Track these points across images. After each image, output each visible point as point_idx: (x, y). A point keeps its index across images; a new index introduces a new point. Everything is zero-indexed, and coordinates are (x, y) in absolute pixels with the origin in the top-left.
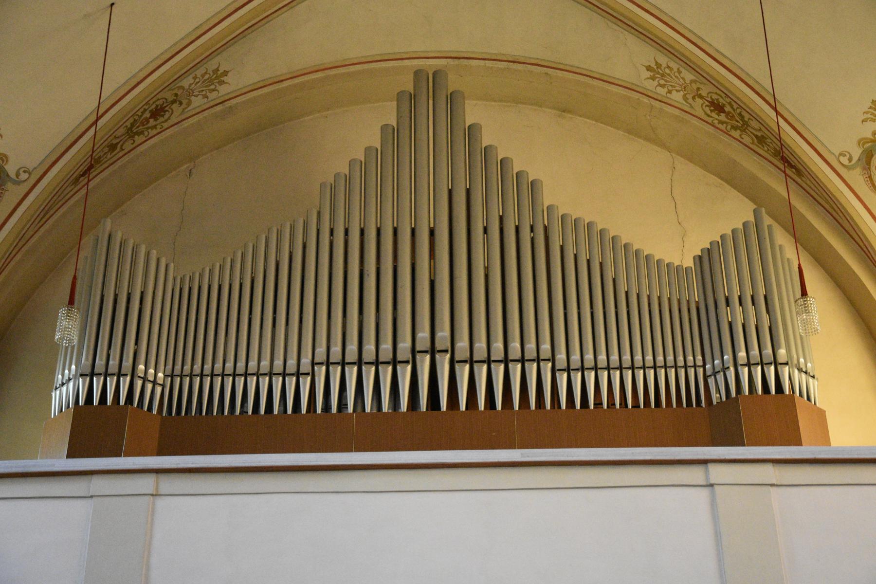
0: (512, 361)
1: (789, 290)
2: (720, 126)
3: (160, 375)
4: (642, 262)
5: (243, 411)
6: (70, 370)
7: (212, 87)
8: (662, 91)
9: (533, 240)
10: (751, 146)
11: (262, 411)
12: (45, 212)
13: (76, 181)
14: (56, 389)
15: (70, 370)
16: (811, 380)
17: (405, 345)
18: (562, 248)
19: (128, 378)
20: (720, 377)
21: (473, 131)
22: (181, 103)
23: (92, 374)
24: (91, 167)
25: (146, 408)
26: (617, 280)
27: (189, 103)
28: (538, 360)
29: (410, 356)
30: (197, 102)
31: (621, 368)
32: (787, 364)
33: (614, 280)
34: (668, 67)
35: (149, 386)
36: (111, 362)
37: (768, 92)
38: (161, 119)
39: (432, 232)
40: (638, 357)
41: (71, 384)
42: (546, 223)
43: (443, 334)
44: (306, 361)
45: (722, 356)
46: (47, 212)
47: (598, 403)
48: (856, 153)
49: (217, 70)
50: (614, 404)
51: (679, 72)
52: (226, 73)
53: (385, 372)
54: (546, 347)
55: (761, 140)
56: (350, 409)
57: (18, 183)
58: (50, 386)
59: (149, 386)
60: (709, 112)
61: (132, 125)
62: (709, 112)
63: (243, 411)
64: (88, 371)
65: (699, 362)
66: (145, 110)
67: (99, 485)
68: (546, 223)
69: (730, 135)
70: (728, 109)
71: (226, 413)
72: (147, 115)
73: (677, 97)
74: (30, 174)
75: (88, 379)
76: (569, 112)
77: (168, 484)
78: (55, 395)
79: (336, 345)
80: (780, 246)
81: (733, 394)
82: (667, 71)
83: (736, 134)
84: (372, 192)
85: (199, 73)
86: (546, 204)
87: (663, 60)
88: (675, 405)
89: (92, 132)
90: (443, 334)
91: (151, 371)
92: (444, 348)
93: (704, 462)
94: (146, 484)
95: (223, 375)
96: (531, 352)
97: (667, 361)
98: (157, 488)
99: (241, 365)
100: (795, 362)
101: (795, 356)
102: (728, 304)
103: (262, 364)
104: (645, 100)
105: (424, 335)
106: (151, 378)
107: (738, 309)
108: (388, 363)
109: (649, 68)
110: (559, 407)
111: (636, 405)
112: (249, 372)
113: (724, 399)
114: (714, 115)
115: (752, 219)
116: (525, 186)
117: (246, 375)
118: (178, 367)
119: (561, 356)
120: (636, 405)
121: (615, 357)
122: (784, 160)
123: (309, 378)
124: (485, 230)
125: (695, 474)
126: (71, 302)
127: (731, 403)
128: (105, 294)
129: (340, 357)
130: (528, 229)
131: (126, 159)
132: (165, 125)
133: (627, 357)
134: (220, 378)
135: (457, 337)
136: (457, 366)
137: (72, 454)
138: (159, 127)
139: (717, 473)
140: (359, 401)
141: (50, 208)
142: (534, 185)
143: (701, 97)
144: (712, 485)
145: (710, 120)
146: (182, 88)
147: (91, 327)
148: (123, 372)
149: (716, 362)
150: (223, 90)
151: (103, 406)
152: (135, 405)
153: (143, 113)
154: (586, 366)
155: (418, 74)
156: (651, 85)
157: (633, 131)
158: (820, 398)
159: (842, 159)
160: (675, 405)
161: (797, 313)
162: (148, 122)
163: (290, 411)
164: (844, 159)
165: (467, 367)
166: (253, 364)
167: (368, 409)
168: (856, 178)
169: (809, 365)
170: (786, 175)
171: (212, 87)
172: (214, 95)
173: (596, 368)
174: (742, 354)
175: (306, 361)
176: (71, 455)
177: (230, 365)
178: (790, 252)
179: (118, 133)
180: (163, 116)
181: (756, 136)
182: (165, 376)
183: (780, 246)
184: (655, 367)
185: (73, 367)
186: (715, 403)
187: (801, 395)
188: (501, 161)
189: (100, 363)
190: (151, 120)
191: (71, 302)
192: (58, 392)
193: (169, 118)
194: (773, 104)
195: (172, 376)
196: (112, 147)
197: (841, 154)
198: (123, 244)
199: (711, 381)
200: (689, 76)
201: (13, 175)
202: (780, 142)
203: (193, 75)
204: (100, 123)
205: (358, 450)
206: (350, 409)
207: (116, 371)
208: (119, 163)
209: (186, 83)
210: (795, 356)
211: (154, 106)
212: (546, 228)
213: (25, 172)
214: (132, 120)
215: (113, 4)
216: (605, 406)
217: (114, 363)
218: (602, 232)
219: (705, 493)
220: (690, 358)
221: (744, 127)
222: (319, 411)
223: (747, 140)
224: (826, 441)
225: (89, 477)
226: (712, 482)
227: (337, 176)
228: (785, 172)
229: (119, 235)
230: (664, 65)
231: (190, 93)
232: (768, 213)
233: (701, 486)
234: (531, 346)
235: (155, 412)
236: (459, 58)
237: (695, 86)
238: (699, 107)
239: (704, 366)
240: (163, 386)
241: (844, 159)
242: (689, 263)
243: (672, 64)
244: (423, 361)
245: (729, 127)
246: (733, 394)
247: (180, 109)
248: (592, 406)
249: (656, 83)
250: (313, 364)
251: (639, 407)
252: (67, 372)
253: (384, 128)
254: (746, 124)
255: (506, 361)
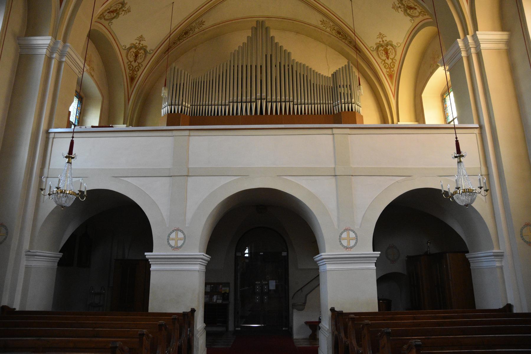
0: (268, 102)
1: (355, 84)
2: (340, 38)
3: (189, 105)
4: (318, 76)
5: (211, 115)
6: (166, 104)
7: (201, 26)
8: (324, 28)
9: (288, 69)
10: (348, 44)
11: (216, 115)
12: (157, 62)
13: (165, 53)
14: (163, 109)
15: (166, 104)
16: (360, 108)
17: (254, 97)
18: (296, 71)
19: (181, 106)
20: (337, 107)
21: (272, 38)
22: (192, 31)
23: (171, 105)
24: (169, 49)
25: (186, 114)
26: (311, 80)
27: (195, 30)
28: (289, 102)
29: (255, 100)
30: (197, 30)
31: (320, 104)
32: (354, 103)
33: (310, 80)
34: (326, 21)
35: (186, 108)
36: (176, 102)
37: (352, 29)
38: (187, 35)
39: (261, 67)
40: (316, 101)
41: (166, 108)
42: (292, 64)
43: (264, 94)
44: (227, 101)
45: (338, 101)
46: (158, 62)
47: (305, 113)
48: (375, 47)
49: (202, 21)
50: (309, 114)
51: (329, 23)
52: (204, 22)
53: (239, 104)
54: (291, 98)
55: (350, 42)
56: (239, 115)
57: (150, 53)
58: (161, 108)
59: (186, 108)
60: (337, 34)
61: (179, 37)
62: (337, 34)
63: (211, 115)
64: (170, 104)
65: (332, 103)
66: (183, 33)
67: (175, 133)
68: (292, 64)
69: (342, 41)
70: (342, 33)
71: (206, 115)
72: (183, 34)
73: (328, 29)
74: (153, 51)
75: (170, 106)
76: (299, 33)
77: (192, 133)
78: (162, 111)
79: (235, 97)
80: (354, 72)
81: (340, 111)
82: (326, 22)
83: (344, 40)
84: (245, 55)
85: (197, 22)
86: (292, 59)
87: (325, 19)
88: (325, 114)
89: (169, 39)
90: (264, 94)
91: (187, 104)
92: (264, 98)
93: (332, 128)
94: (187, 133)
95: (205, 105)
96: (274, 100)
97: (298, 102)
98: (190, 134)
99: (210, 102)
100: (356, 103)
101: (356, 101)
102: (340, 87)
103: (216, 102)
104: (320, 30)
105: (259, 95)
106: (187, 106)
107: (343, 89)
108: (249, 102)
109: (321, 21)
110: (295, 114)
111: (315, 114)
112: (206, 105)
113: (338, 112)
114: (338, 35)
115: (347, 64)
116: (302, 65)
117: (211, 105)
118: (194, 103)
119: (295, 101)
120: (315, 114)
121: (310, 101)
122: (356, 48)
123: (228, 106)
124: (276, 66)
125: (329, 131)
126: (165, 86)
127: (339, 114)
128: (174, 83)
129: (236, 100)
130: (287, 66)
131: (178, 46)
132: (188, 37)
133: (313, 101)
134: (205, 106)
135: (268, 95)
136: (268, 103)
137: (168, 125)
138: (186, 37)
139: (335, 131)
140: (242, 112)
141: (159, 60)
142: (289, 53)
143: (335, 30)
144: (333, 134)
145: (337, 36)
146: (192, 26)
147: (171, 92)
148: (179, 104)
149: (336, 103)
150: (204, 27)
151: (175, 113)
152: (183, 113)
153: (182, 33)
154: (234, 101)
155: (257, 21)
156: (321, 26)
157: (316, 39)
158: (362, 113)
159: (371, 48)
160: (325, 114)
161: (358, 90)
162: (183, 36)
163: (223, 115)
164: (372, 49)
165: (270, 103)
166: (213, 102)
167: (244, 114)
168: (374, 54)
169: (360, 104)
170: (357, 53)
171: (201, 26)
172: (201, 28)
173: (314, 104)
174: (343, 101)
175: (227, 101)
176: (167, 125)
177: (207, 102)
178: (357, 73)
179: (176, 39)
180: (187, 34)
181: (349, 41)
182: (190, 105)
183: (354, 72)
184: (320, 104)
185: (167, 103)
186: (335, 113)
187: (357, 112)
188: (284, 50)
189: (173, 102)
190: (184, 35)
191: (165, 86)
192: (163, 110)
193: (189, 35)
194: (354, 32)
195: (192, 105)
196: (174, 43)
197: (371, 47)
198: (181, 71)
199: (335, 108)
200: (331, 24)
201: (149, 52)
202: (354, 34)
203: (195, 22)
204: (171, 36)
205: (242, 124)
206: (239, 115)
207: (177, 104)
208: (177, 47)
209: (194, 24)
210: (356, 101)
211: (185, 31)
212: (292, 66)
213: (152, 50)
214: (179, 35)
215: (173, 3)
216: (307, 114)
217: (177, 102)
218: (307, 67)
219: (331, 136)
220: (329, 101)
221: (346, 39)
222: (231, 115)
223: (347, 42)
224: (363, 123)
225: (172, 131)
226: (334, 133)
227: (235, 50)
228: (356, 51)
229: (177, 67)
230: (325, 20)
231: (195, 28)
232: (352, 63)
233: (331, 134)
234: (274, 97)
235: (188, 115)
236: (268, 17)
237: (333, 27)
238: (334, 32)
239: (333, 104)
240: (190, 108)
241: (372, 49)
242: (330, 76)
243: (327, 20)
244: (258, 102)
245: (342, 38)
246: (340, 111)
247: (192, 32)
248: (303, 114)
249: (323, 25)
250: (229, 102)
251: (315, 114)
252: (165, 104)
253: (248, 37)
254: (347, 38)
255: (281, 102)
